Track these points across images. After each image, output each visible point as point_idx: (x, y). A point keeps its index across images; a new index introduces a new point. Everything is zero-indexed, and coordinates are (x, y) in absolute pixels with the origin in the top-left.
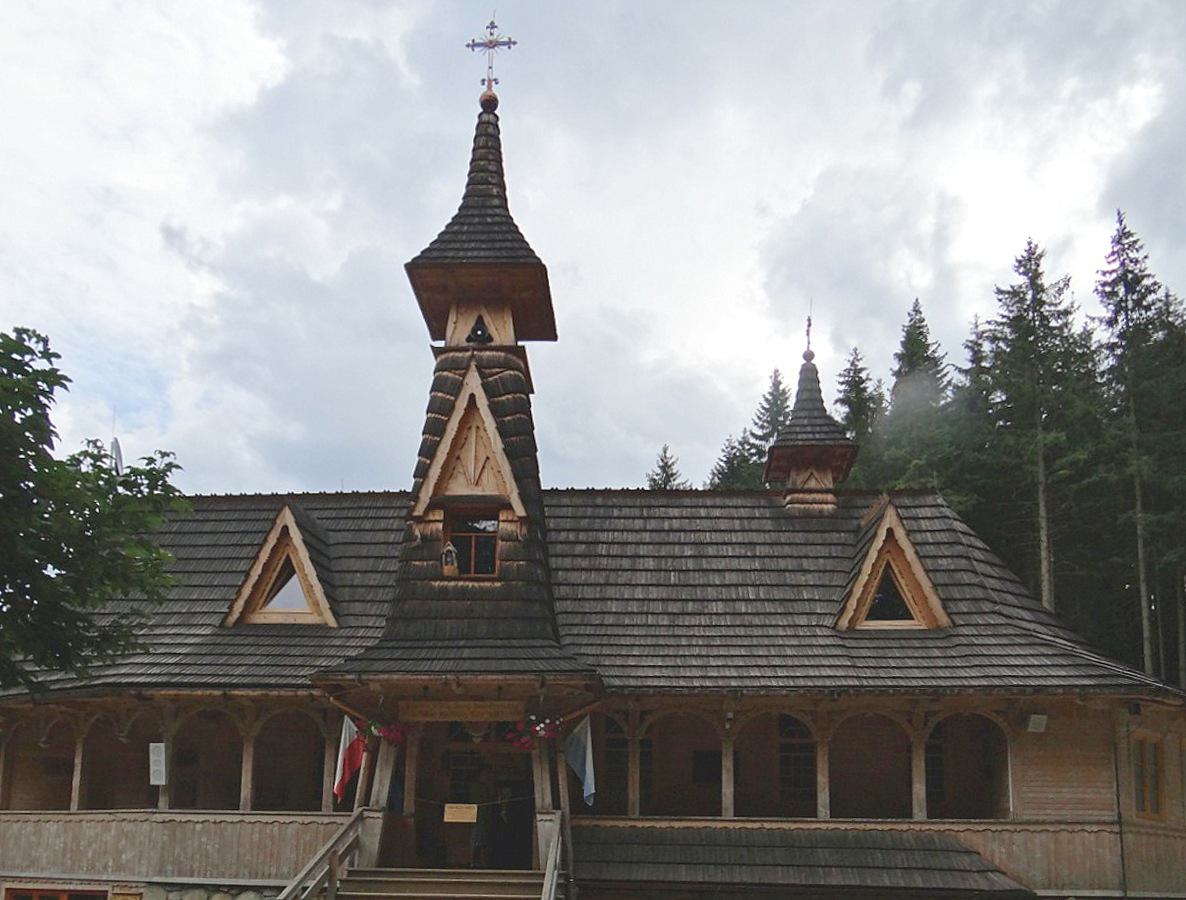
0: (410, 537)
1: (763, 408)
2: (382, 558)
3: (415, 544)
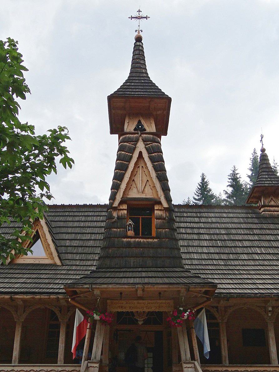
0: (110, 217)
1: (198, 188)
2: (79, 233)
3: (114, 220)
